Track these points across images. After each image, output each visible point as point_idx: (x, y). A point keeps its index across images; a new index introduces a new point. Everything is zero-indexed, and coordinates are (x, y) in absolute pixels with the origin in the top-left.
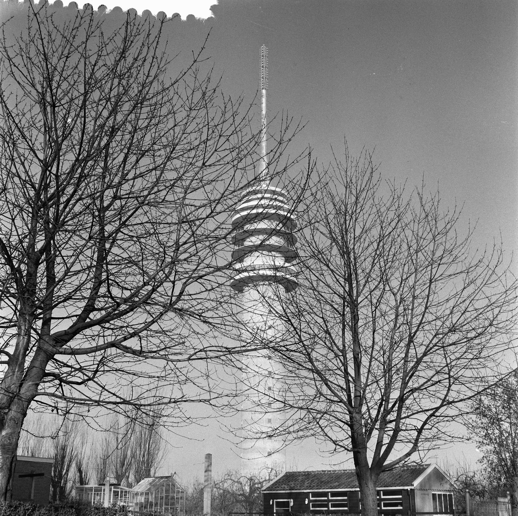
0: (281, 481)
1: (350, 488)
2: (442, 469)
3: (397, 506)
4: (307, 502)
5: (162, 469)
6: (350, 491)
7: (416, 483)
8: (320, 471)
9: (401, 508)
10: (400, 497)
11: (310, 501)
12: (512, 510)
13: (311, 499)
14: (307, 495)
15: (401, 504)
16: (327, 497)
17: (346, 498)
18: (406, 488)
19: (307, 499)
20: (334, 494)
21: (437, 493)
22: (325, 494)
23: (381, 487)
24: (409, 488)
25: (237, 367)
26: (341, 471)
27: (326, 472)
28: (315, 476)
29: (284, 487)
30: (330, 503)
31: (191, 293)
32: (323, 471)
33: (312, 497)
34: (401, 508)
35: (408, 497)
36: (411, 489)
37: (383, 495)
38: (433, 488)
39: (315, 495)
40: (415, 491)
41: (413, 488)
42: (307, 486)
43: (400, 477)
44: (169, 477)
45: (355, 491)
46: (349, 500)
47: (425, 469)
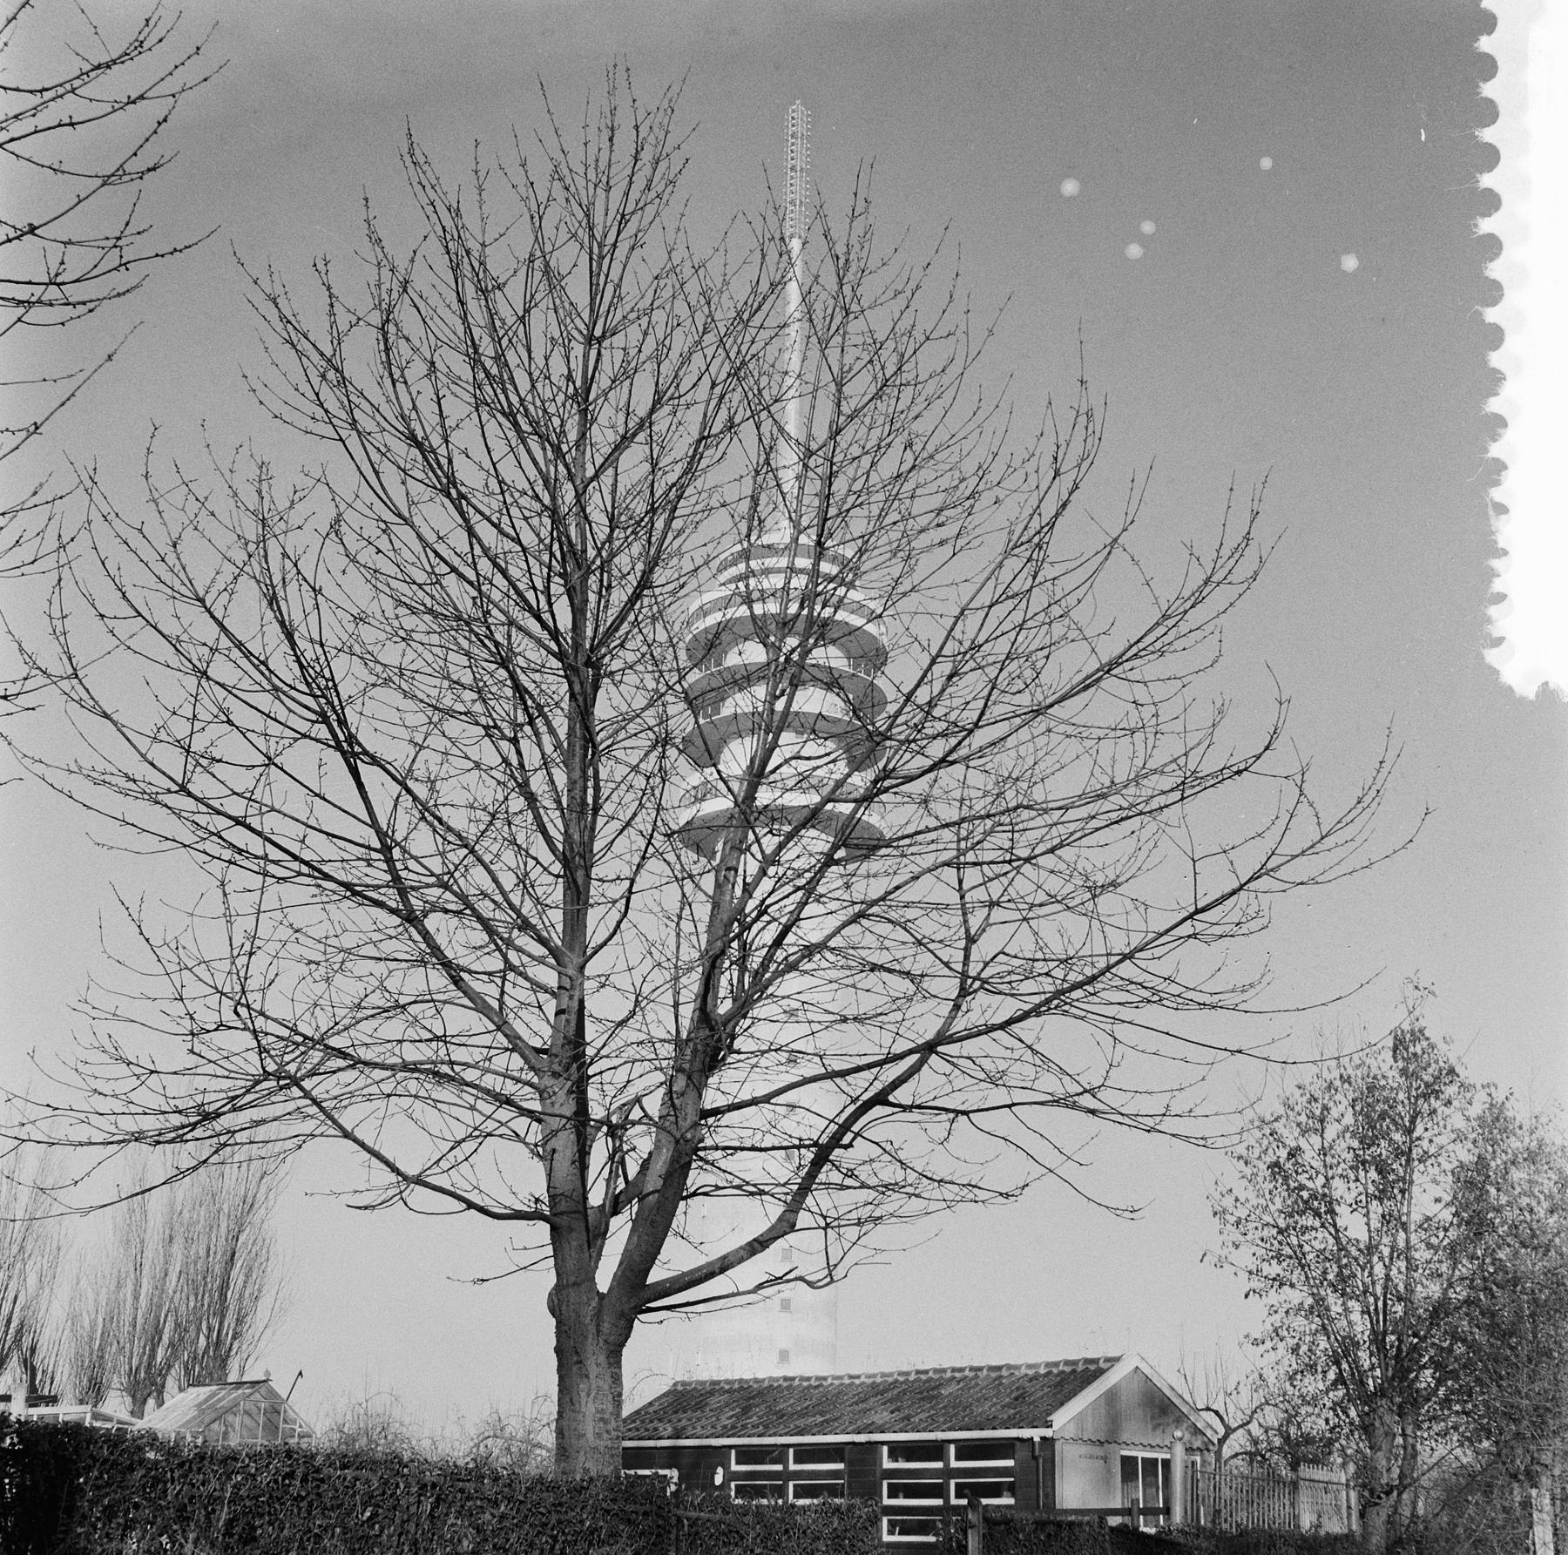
0: (651, 1410)
1: (853, 1432)
2: (1168, 1378)
3: (999, 1495)
4: (718, 1480)
5: (250, 1364)
6: (853, 1443)
7: (1063, 1419)
8: (777, 1380)
9: (1011, 1501)
10: (1010, 1463)
11: (730, 1476)
12: (1362, 1515)
13: (734, 1467)
14: (720, 1454)
15: (1012, 1489)
16: (785, 1462)
17: (841, 1466)
18: (1026, 1433)
19: (720, 1470)
20: (805, 1454)
21: (1141, 1454)
22: (934, 1450)
23: (950, 1429)
24: (1036, 1434)
25: (115, 723)
26: (841, 1378)
27: (797, 1382)
28: (760, 1393)
29: (656, 1429)
30: (791, 1484)
31: (828, 1084)
32: (786, 1379)
33: (958, 1458)
34: (1011, 1501)
35: (1033, 1463)
36: (1043, 1439)
37: (738, 1463)
38: (1125, 1437)
39: (746, 1454)
40: (1058, 1446)
41: (1048, 1433)
42: (725, 1427)
43: (1016, 1399)
44: (258, 1382)
45: (869, 1443)
46: (852, 1473)
47: (1101, 1372)
